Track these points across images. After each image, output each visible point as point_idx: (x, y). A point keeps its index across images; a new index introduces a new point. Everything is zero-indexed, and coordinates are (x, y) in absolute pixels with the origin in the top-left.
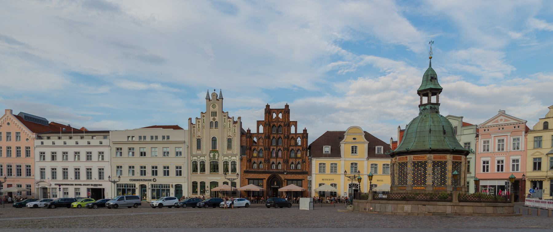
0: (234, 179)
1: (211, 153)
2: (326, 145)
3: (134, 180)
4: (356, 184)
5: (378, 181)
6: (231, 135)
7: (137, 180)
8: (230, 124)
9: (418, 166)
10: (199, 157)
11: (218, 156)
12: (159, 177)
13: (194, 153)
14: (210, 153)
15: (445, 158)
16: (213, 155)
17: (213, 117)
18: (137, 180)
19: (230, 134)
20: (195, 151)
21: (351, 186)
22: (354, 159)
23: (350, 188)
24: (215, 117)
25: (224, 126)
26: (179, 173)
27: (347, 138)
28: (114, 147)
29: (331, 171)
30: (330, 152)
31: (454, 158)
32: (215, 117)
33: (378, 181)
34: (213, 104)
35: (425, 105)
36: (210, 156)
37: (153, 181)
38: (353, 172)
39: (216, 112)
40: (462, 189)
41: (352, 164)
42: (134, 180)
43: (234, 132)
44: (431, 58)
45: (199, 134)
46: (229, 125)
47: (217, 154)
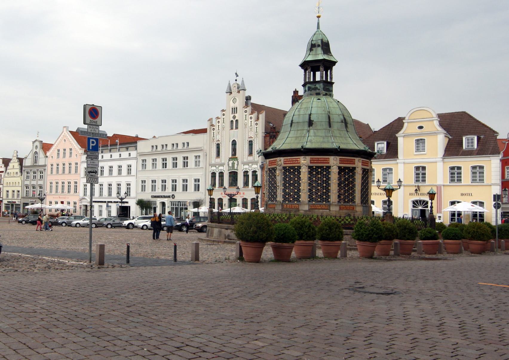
0: (234, 195)
1: (230, 161)
2: (379, 140)
3: (155, 197)
4: (424, 201)
5: (462, 195)
6: (252, 136)
7: (158, 197)
8: (251, 121)
9: (318, 173)
10: (217, 166)
11: (238, 165)
12: (178, 193)
13: (213, 162)
14: (229, 160)
15: (299, 162)
16: (232, 164)
17: (233, 115)
18: (158, 197)
19: (252, 134)
20: (214, 160)
21: (415, 203)
22: (420, 160)
23: (414, 207)
24: (236, 115)
25: (245, 124)
26: (197, 188)
27: (407, 128)
28: (140, 159)
29: (474, 180)
30: (385, 151)
31: (341, 161)
32: (236, 115)
33: (462, 195)
34: (233, 98)
35: (318, 82)
36: (228, 164)
37: (171, 198)
38: (476, 180)
39: (237, 108)
40: (330, 207)
41: (417, 168)
42: (155, 197)
43: (255, 131)
44: (319, 17)
45: (218, 137)
46: (250, 122)
47: (236, 162)
